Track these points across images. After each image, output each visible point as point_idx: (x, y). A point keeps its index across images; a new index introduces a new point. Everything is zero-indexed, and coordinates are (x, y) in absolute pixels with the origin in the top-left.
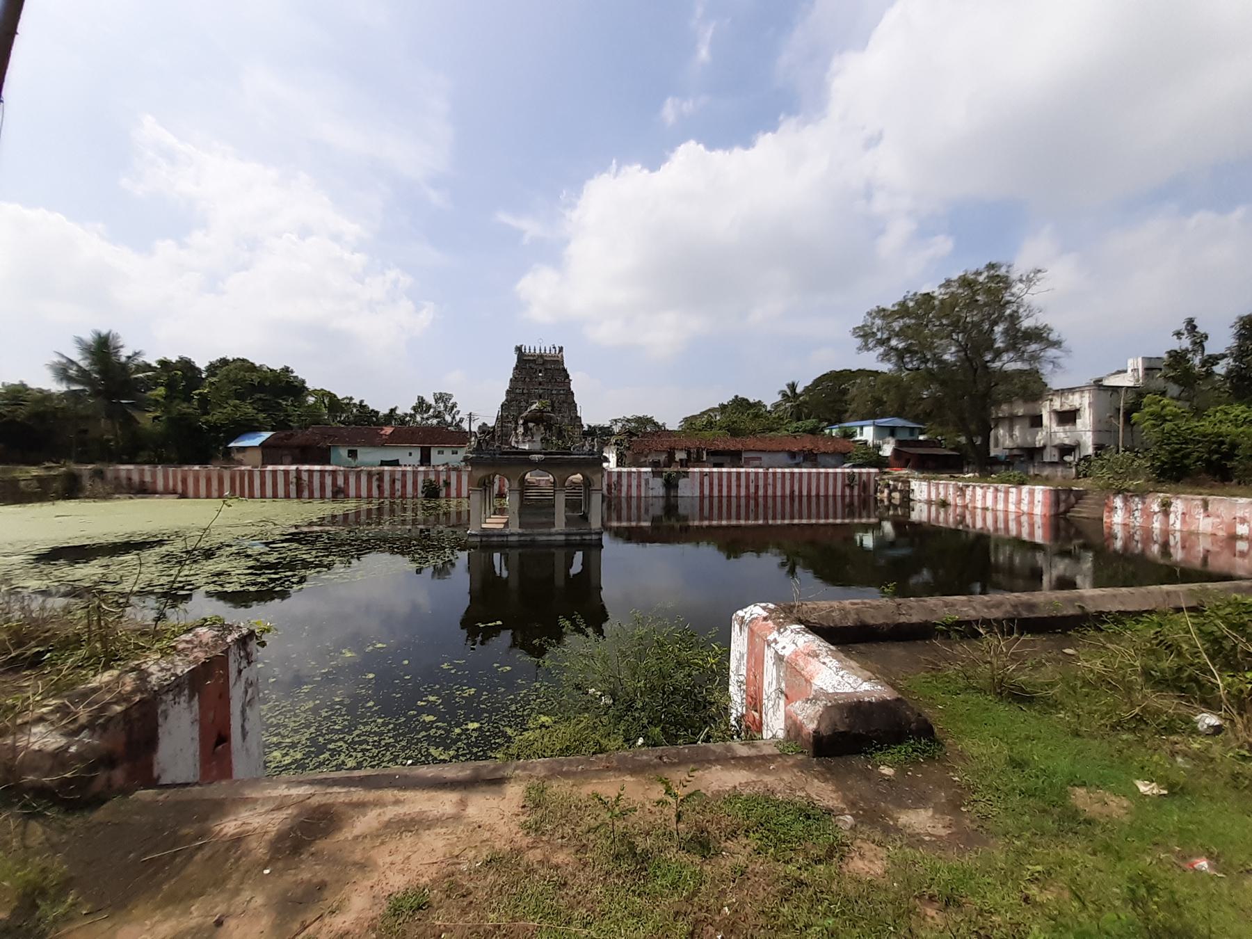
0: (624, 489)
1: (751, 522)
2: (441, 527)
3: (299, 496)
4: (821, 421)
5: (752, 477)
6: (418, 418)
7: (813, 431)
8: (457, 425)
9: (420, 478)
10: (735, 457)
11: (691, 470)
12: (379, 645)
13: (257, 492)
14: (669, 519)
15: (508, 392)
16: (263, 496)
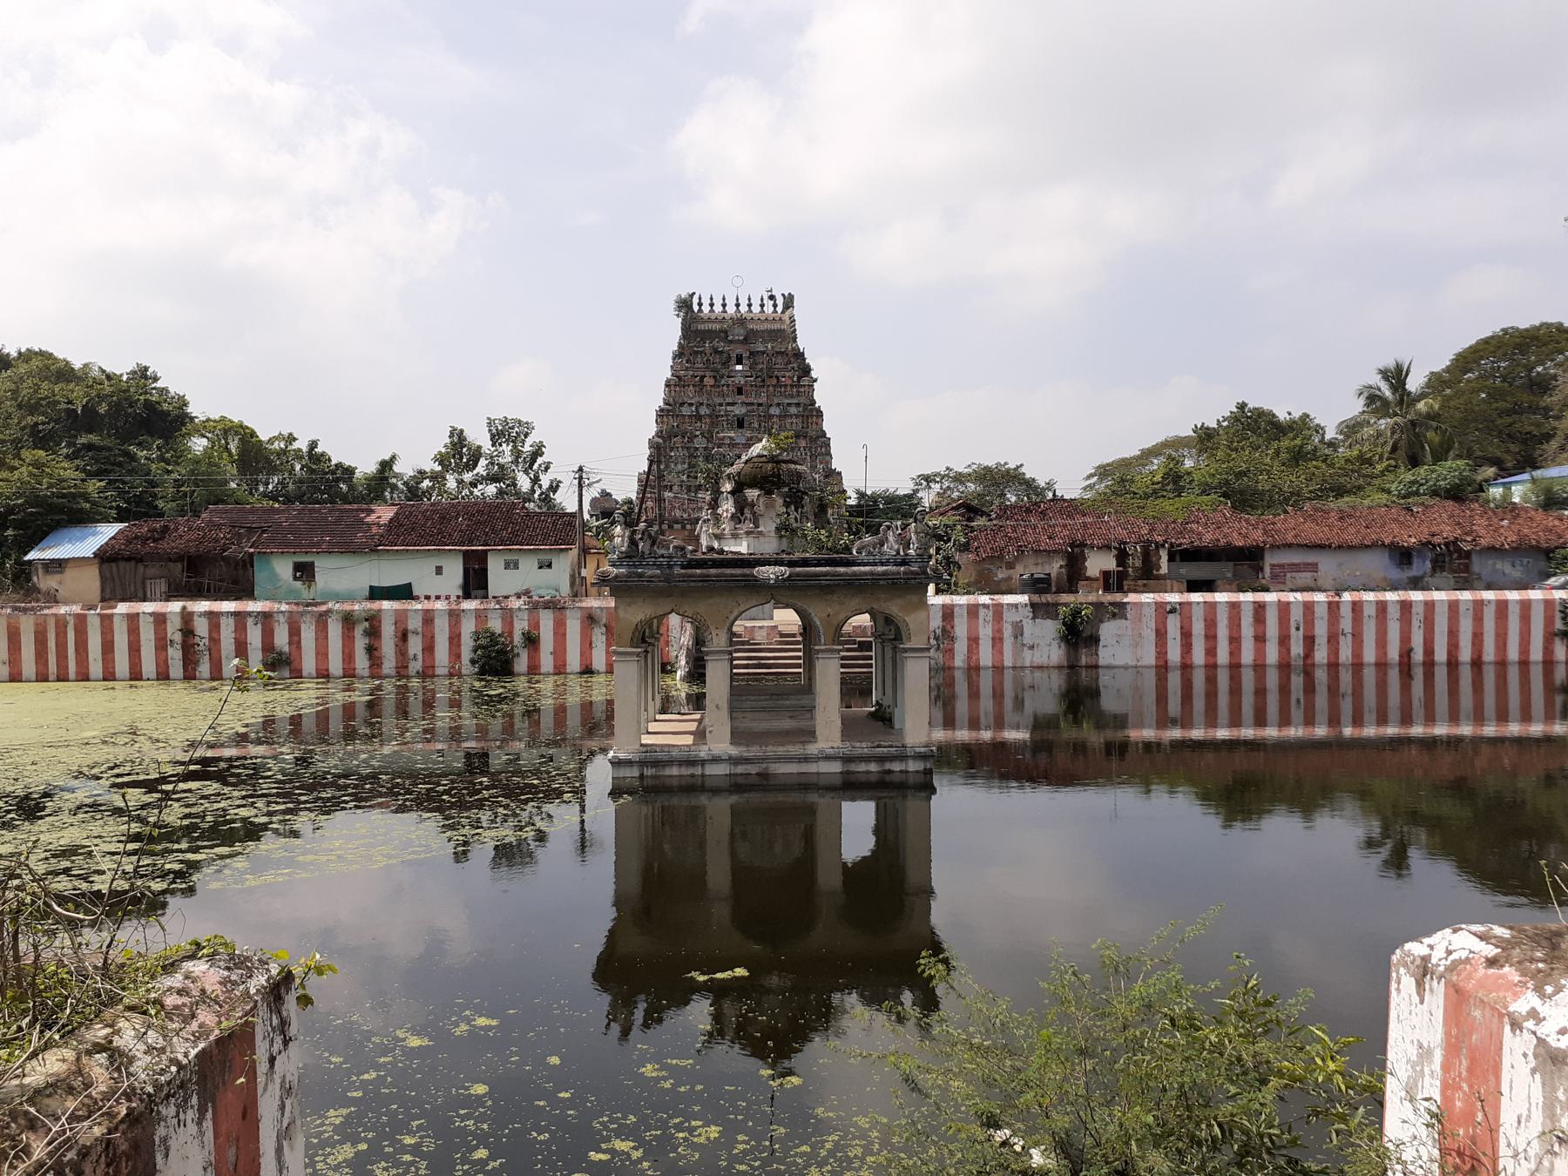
0: (961, 648)
1: (1295, 732)
2: (519, 746)
3: (189, 676)
4: (1479, 463)
5: (1296, 615)
6: (451, 483)
7: (1457, 494)
8: (546, 499)
9: (468, 628)
10: (1245, 564)
11: (1132, 598)
12: (482, 1021)
13: (96, 668)
14: (1077, 722)
15: (661, 414)
16: (109, 676)
